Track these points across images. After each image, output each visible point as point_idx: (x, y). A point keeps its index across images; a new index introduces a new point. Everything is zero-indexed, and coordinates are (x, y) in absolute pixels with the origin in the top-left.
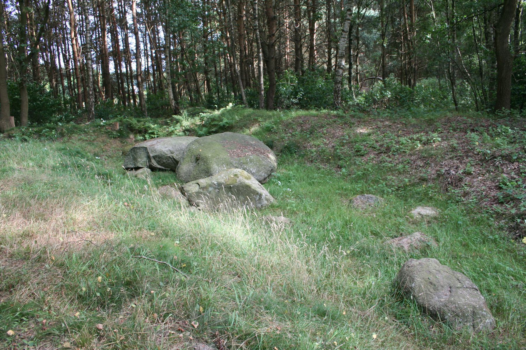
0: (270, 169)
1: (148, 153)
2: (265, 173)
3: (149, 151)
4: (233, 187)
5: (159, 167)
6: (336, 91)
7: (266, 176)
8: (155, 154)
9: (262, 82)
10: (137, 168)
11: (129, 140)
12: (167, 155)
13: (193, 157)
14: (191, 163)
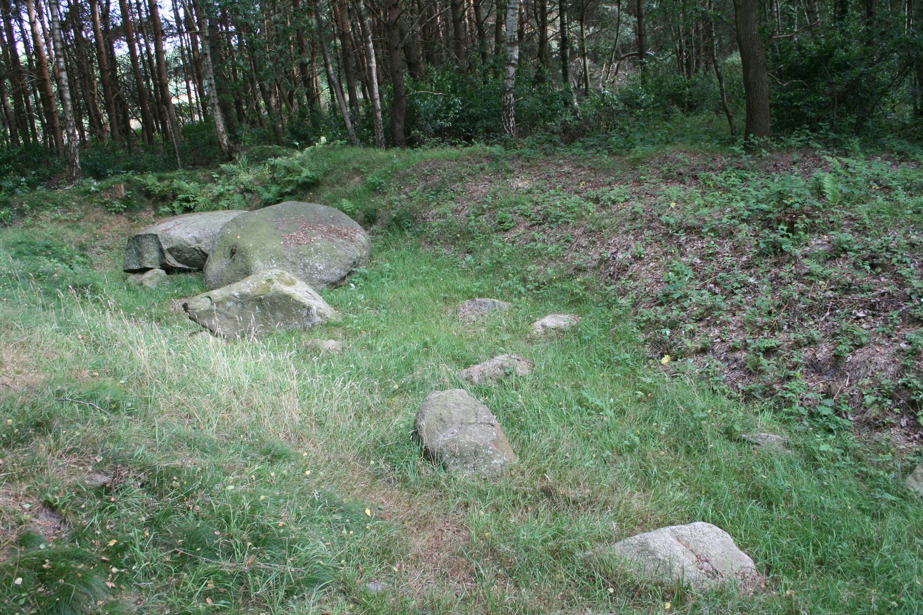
0: (351, 262)
1: (159, 243)
2: (341, 269)
3: (161, 241)
4: (265, 298)
5: (180, 265)
6: (506, 107)
7: (344, 273)
8: (171, 245)
9: (377, 96)
10: (144, 270)
11: (143, 214)
12: (190, 245)
13: (227, 248)
14: (224, 260)
